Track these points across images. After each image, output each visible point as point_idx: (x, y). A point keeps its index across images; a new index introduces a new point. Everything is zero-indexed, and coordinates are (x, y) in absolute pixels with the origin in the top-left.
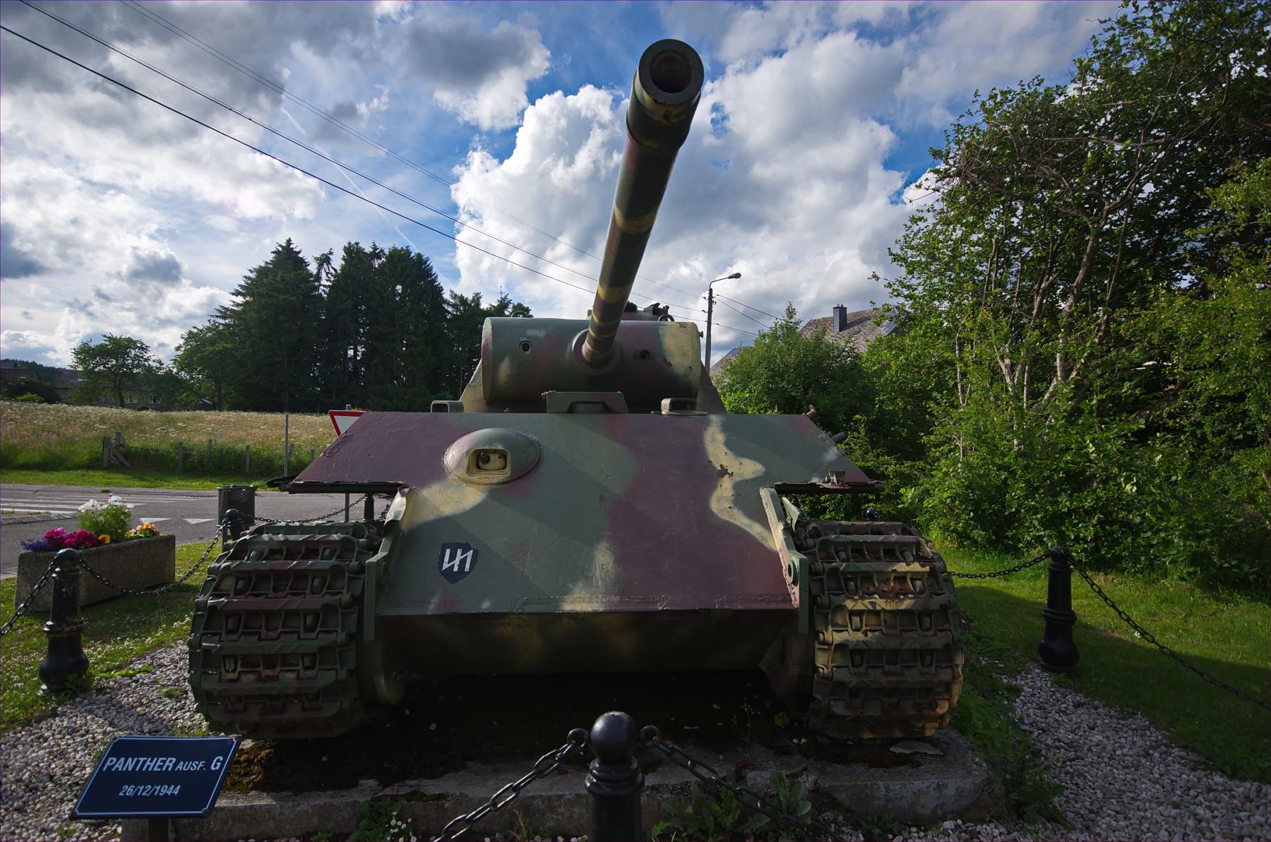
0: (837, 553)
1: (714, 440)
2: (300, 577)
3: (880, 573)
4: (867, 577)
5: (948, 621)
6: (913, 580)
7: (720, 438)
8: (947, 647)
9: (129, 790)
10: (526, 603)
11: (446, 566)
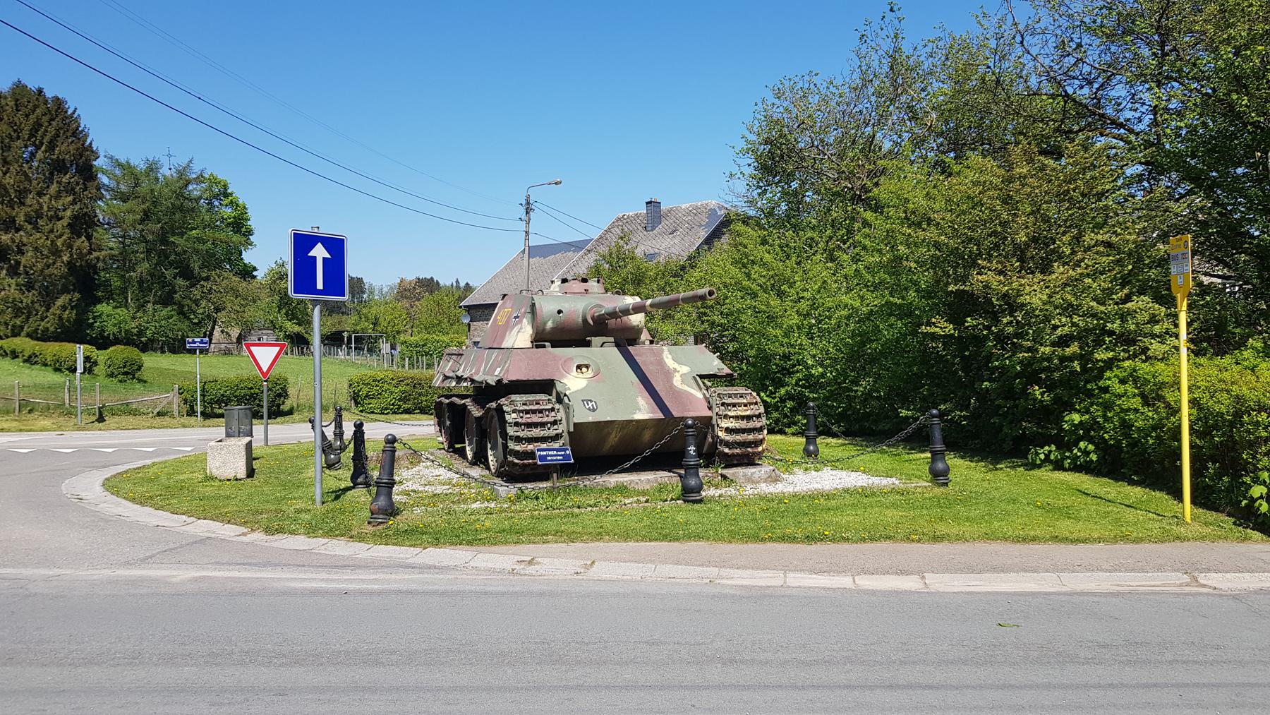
1: (667, 358)
2: (541, 411)
7: (670, 356)
8: (761, 427)
9: (549, 458)
10: (1077, 576)
11: (593, 403)
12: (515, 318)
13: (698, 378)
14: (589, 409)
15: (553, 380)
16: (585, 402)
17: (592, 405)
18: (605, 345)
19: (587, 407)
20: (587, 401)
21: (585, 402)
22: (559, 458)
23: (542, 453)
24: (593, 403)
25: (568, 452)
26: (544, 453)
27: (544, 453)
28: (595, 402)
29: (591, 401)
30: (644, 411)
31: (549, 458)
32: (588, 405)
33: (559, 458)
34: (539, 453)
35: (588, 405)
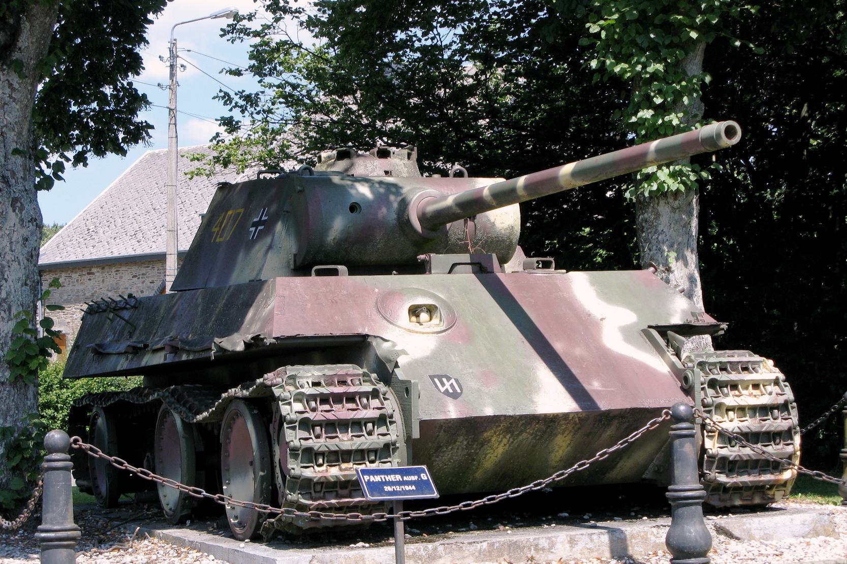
0: (710, 370)
2: (351, 398)
3: (742, 381)
4: (734, 386)
5: (789, 414)
6: (764, 386)
9: (388, 488)
11: (453, 381)
12: (256, 225)
13: (655, 333)
14: (446, 392)
15: (366, 336)
16: (436, 380)
17: (452, 385)
18: (458, 268)
19: (443, 390)
20: (440, 377)
21: (436, 380)
22: (407, 488)
23: (372, 478)
24: (453, 381)
25: (424, 477)
26: (377, 478)
27: (377, 478)
28: (457, 381)
29: (449, 379)
30: (336, 418)
31: (388, 488)
32: (443, 384)
33: (407, 488)
34: (366, 478)
35: (443, 384)
